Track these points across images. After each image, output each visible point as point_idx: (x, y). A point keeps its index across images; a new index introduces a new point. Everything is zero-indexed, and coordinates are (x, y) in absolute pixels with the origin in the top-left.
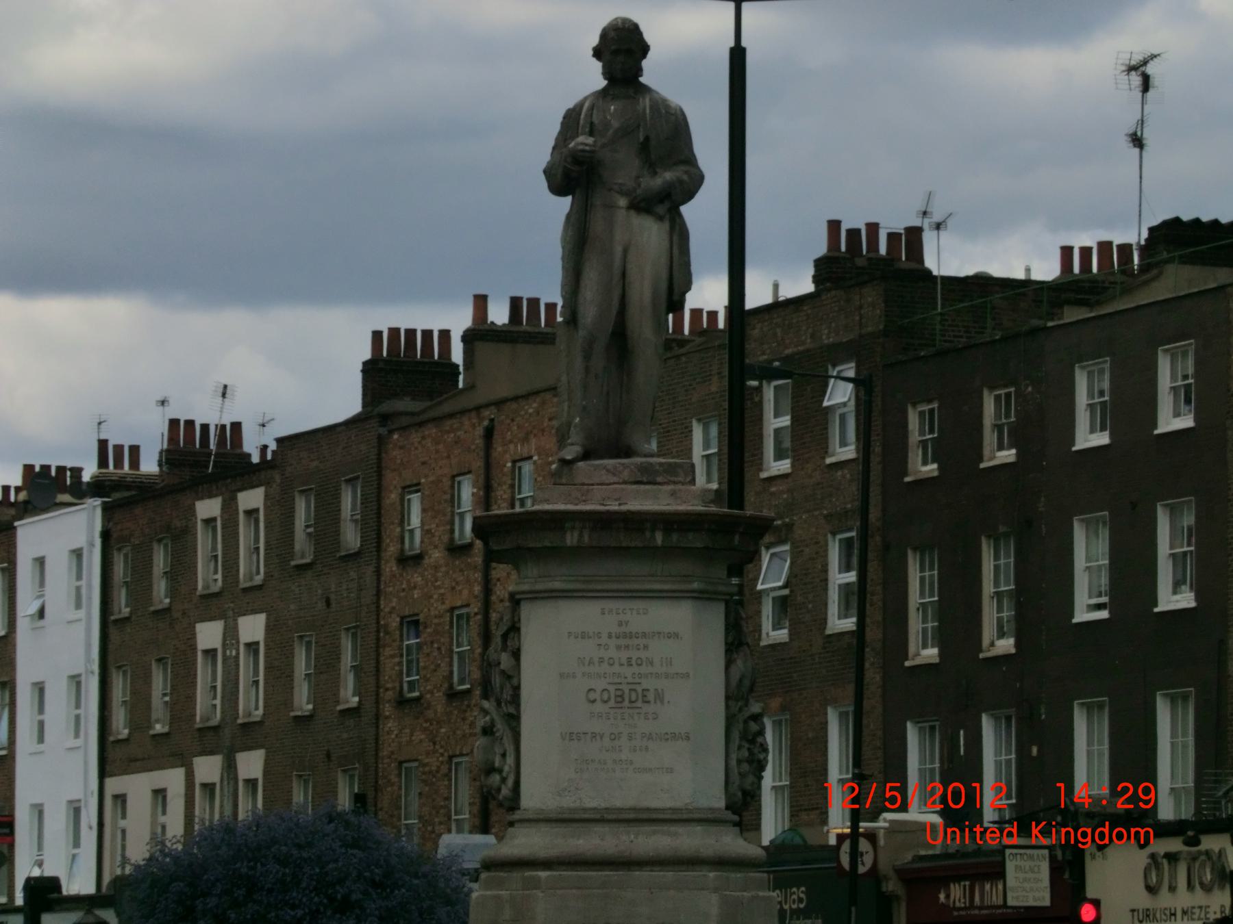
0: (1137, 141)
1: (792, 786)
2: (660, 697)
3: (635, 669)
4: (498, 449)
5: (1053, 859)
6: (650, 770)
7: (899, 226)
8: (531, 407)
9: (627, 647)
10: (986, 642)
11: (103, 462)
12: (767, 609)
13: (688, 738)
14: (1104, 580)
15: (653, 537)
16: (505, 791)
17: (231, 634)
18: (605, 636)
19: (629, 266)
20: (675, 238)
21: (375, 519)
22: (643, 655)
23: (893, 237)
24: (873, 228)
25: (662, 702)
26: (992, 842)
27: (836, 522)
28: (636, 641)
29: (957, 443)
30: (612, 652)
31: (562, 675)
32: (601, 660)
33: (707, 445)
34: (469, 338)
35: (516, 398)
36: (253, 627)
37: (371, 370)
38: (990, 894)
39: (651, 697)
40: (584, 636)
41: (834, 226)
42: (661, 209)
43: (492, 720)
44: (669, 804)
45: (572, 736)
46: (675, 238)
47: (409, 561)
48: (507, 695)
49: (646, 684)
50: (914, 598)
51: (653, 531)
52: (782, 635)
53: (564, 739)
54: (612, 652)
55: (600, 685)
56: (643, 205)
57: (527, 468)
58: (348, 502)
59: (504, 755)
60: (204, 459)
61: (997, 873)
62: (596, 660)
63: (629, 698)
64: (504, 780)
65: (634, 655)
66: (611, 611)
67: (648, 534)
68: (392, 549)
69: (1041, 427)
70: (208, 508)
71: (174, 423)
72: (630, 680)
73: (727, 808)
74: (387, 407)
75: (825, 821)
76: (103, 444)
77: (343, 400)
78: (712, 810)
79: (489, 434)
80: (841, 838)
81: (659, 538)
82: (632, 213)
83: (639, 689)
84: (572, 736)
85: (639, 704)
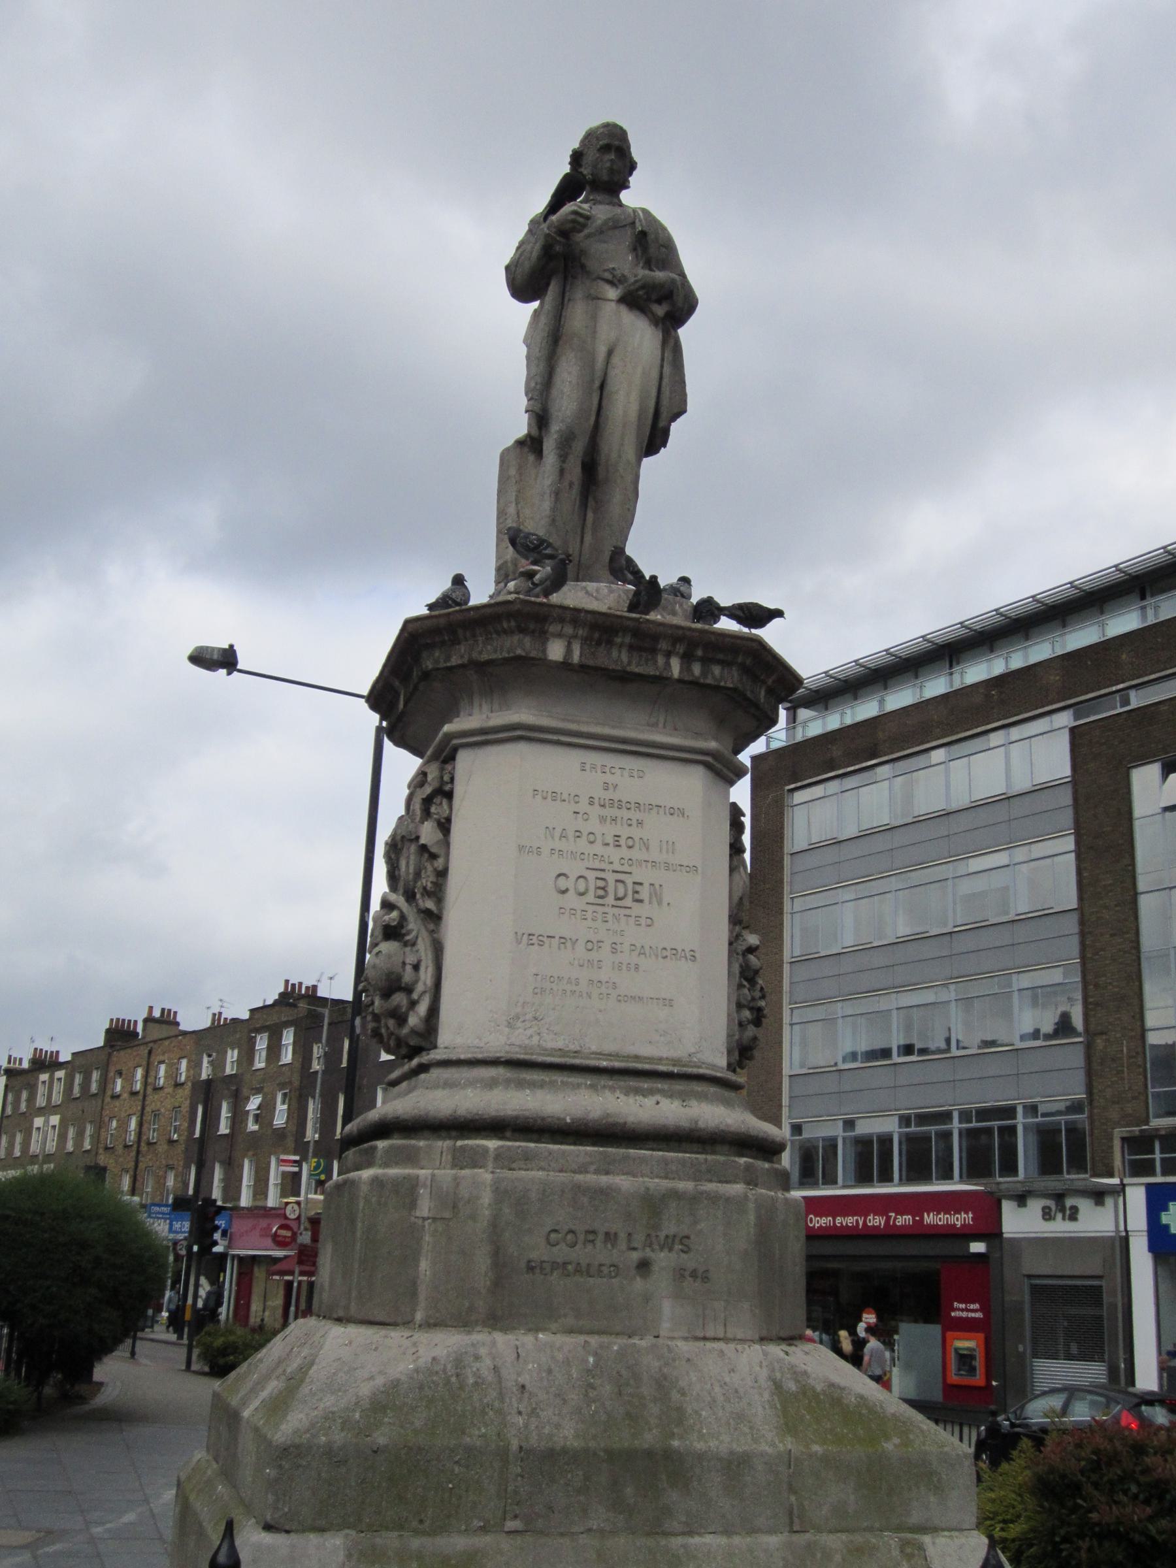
1: (282, 1184)
2: (657, 895)
3: (624, 852)
6: (641, 999)
7: (310, 984)
8: (167, 1043)
9: (614, 820)
11: (9, 1062)
12: (251, 1119)
15: (668, 664)
16: (413, 1020)
17: (47, 1122)
18: (584, 801)
19: (612, 373)
21: (104, 1083)
22: (636, 833)
23: (307, 988)
24: (300, 984)
25: (660, 903)
27: (282, 1086)
28: (625, 814)
30: (593, 825)
31: (521, 848)
32: (578, 834)
34: (146, 1021)
36: (55, 1120)
37: (108, 1031)
39: (644, 894)
41: (287, 982)
42: (660, 310)
43: (403, 917)
45: (534, 939)
47: (116, 1097)
48: (427, 880)
49: (644, 875)
50: (310, 1115)
51: (668, 655)
52: (256, 1128)
53: (519, 942)
54: (593, 825)
55: (575, 868)
58: (95, 1076)
59: (416, 967)
60: (44, 1063)
63: (614, 892)
64: (413, 1004)
66: (593, 767)
67: (661, 660)
68: (109, 1093)
70: (44, 1077)
71: (36, 1049)
76: (10, 1057)
77: (100, 1041)
78: (713, 1067)
79: (150, 1052)
81: (676, 667)
82: (623, 309)
83: (629, 880)
84: (534, 939)
85: (628, 902)
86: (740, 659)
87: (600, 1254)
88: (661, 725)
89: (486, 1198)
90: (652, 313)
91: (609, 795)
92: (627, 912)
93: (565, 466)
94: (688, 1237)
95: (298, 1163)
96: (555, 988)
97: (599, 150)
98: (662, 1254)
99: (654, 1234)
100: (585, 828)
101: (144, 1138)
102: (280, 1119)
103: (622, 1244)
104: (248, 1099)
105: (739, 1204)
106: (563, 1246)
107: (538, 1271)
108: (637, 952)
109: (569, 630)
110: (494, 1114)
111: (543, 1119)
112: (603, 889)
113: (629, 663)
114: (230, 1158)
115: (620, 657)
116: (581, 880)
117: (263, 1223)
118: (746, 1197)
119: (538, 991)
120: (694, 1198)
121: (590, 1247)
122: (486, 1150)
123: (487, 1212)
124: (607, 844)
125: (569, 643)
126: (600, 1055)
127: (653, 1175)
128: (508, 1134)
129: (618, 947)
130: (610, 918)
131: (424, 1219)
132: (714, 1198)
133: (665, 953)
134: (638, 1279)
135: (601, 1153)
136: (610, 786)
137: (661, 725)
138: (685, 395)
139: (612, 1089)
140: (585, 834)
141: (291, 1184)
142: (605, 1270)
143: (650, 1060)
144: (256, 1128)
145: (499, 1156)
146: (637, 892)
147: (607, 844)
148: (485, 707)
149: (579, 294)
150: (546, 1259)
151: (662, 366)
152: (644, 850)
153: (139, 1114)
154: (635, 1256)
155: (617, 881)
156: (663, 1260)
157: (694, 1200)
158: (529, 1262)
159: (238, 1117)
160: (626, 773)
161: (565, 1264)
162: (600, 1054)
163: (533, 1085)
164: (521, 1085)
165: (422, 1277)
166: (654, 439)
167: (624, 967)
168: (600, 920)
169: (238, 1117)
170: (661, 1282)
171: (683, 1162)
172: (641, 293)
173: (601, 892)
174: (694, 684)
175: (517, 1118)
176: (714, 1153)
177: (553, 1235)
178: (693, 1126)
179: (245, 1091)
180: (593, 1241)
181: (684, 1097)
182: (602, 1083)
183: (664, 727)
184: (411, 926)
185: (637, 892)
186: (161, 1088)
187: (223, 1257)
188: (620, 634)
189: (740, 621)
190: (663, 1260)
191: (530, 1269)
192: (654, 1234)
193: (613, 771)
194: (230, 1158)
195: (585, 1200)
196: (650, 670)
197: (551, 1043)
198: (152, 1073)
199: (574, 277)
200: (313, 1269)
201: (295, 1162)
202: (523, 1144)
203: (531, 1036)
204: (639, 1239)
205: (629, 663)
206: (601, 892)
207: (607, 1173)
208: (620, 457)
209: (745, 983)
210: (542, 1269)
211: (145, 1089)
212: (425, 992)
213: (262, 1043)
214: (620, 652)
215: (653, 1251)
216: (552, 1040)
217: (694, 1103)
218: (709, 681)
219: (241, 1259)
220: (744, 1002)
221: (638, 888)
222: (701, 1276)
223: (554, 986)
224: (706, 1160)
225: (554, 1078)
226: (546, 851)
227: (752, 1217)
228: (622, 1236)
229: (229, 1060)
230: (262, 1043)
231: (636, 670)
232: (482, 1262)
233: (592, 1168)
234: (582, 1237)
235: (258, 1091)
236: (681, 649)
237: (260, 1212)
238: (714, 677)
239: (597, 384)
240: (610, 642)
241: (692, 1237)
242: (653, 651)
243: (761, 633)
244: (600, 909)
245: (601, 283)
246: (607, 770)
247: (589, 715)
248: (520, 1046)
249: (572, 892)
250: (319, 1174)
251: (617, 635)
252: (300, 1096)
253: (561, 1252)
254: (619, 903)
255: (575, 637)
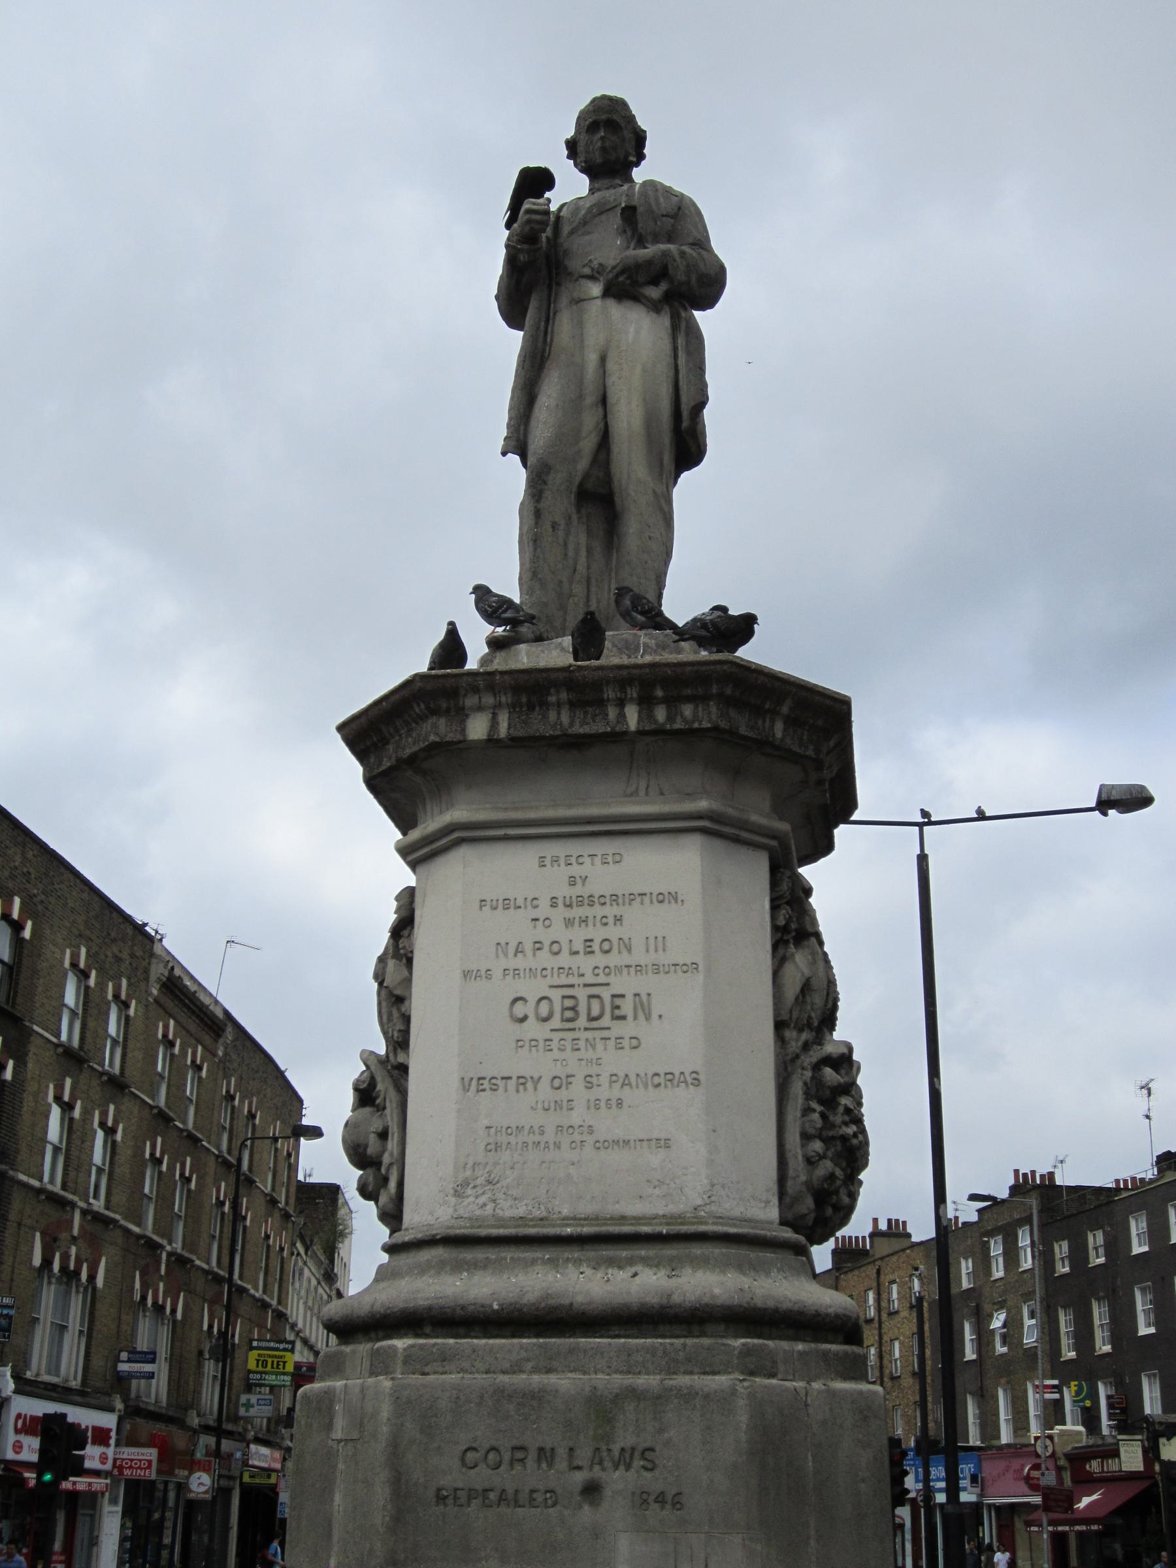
0: (1148, 1117)
1: (1014, 1419)
2: (643, 1007)
3: (600, 959)
4: (882, 1277)
5: (1143, 1446)
6: (626, 1143)
7: (1045, 1172)
8: (894, 1259)
9: (584, 921)
10: (1097, 1348)
13: (697, 1082)
14: (1152, 1316)
15: (622, 716)
18: (544, 903)
20: (681, 341)
22: (613, 932)
23: (1042, 1176)
24: (1033, 1172)
25: (648, 1017)
26: (1110, 1440)
28: (598, 911)
29: (1079, 1255)
30: (558, 931)
31: (466, 974)
32: (538, 946)
33: (967, 1268)
34: (872, 1235)
35: (888, 1256)
38: (1112, 1465)
39: (627, 1007)
40: (507, 904)
41: (1016, 1172)
44: (660, 1208)
46: (681, 341)
49: (623, 984)
50: (1063, 1329)
51: (621, 704)
52: (1005, 1350)
54: (558, 931)
55: (532, 989)
56: (624, 287)
57: (895, 1287)
61: (1115, 1453)
62: (528, 947)
65: (597, 934)
66: (555, 860)
67: (612, 712)
69: (1117, 1244)
72: (589, 979)
73: (783, 1222)
74: (431, 824)
75: (1029, 1431)
79: (878, 1272)
80: (1036, 1438)
81: (632, 717)
82: (611, 303)
83: (606, 994)
85: (606, 1021)
86: (714, 690)
87: (531, 1476)
88: (642, 793)
89: (386, 1411)
90: (645, 297)
91: (578, 890)
92: (605, 1034)
93: (541, 505)
94: (652, 1449)
95: (1058, 1388)
96: (513, 1143)
97: (587, 131)
98: (617, 1473)
99: (604, 1448)
100: (546, 937)
101: (887, 1372)
102: (1030, 1339)
103: (561, 1464)
104: (991, 1316)
105: (726, 1399)
106: (482, 1469)
107: (450, 1501)
108: (619, 1084)
109: (489, 700)
110: (401, 1305)
111: (463, 1308)
112: (573, 1009)
113: (571, 724)
114: (981, 1388)
115: (561, 719)
116: (544, 1002)
117: (1015, 1464)
118: (733, 1392)
119: (492, 1147)
120: (659, 1397)
121: (518, 1467)
122: (394, 1349)
123: (385, 1429)
124: (577, 953)
125: (494, 715)
126: (575, 1219)
127: (610, 1370)
128: (428, 1330)
129: (594, 1080)
130: (582, 1044)
131: (339, 1441)
132: (688, 1396)
133: (657, 1080)
134: (586, 1507)
135: (540, 1346)
136: (579, 880)
137: (642, 793)
138: (704, 386)
139: (578, 1262)
140: (547, 944)
141: (1054, 1413)
142: (539, 1497)
143: (638, 1220)
144: (1005, 1350)
145: (408, 1357)
146: (618, 1007)
147: (577, 953)
148: (436, 810)
149: (564, 301)
150: (461, 1485)
151: (676, 357)
152: (624, 952)
153: (876, 1345)
154: (579, 1477)
155: (591, 997)
156: (617, 1481)
157: (659, 1399)
158: (439, 1490)
159: (984, 1338)
160: (598, 860)
161: (486, 1490)
162: (575, 1218)
163: (473, 1266)
164: (458, 1267)
165: (336, 1514)
166: (686, 447)
167: (603, 1104)
168: (569, 1048)
169: (984, 1338)
170: (615, 1510)
171: (652, 1351)
172: (621, 279)
173: (569, 1014)
174: (659, 732)
175: (430, 1308)
176: (703, 1334)
177: (469, 1455)
178: (664, 1301)
179: (987, 1307)
180: (522, 1460)
181: (674, 1266)
182: (566, 1255)
183: (647, 794)
184: (380, 1087)
185: (618, 1007)
186: (897, 1312)
187: (977, 1507)
188: (552, 691)
189: (702, 643)
190: (617, 1481)
191: (441, 1499)
192: (604, 1448)
193: (581, 860)
194: (981, 1388)
195: (511, 1407)
196: (599, 727)
197: (508, 1210)
198: (884, 1296)
199: (558, 284)
200: (91, 1512)
201: (1054, 1387)
202: (439, 1341)
203: (485, 1205)
204: (584, 1455)
205: (571, 724)
206: (569, 1014)
207: (549, 1371)
208: (629, 477)
209: (814, 1105)
210: (456, 1498)
211: (880, 1316)
212: (391, 1164)
213: (996, 1249)
214: (559, 714)
215: (603, 1469)
216: (511, 1208)
217: (688, 1271)
218: (678, 725)
219: (999, 1509)
220: (811, 1131)
221: (618, 1001)
222: (670, 1500)
223: (512, 1139)
224: (684, 1345)
225: (503, 1255)
226: (497, 973)
227: (743, 1418)
228: (562, 1452)
229: (964, 1271)
230: (996, 1249)
231: (581, 731)
232: (381, 1494)
233: (529, 1366)
234: (507, 1456)
235: (1001, 1305)
236: (633, 692)
237: (1019, 1450)
238: (685, 720)
239: (590, 399)
240: (545, 705)
241: (657, 1449)
242: (601, 703)
243: (745, 653)
244: (570, 1035)
245: (583, 281)
246: (573, 860)
247: (545, 797)
248: (470, 1219)
249: (532, 1019)
250: (1083, 1400)
251: (549, 694)
252: (1049, 1307)
253: (481, 1477)
254: (595, 1024)
255: (498, 706)
